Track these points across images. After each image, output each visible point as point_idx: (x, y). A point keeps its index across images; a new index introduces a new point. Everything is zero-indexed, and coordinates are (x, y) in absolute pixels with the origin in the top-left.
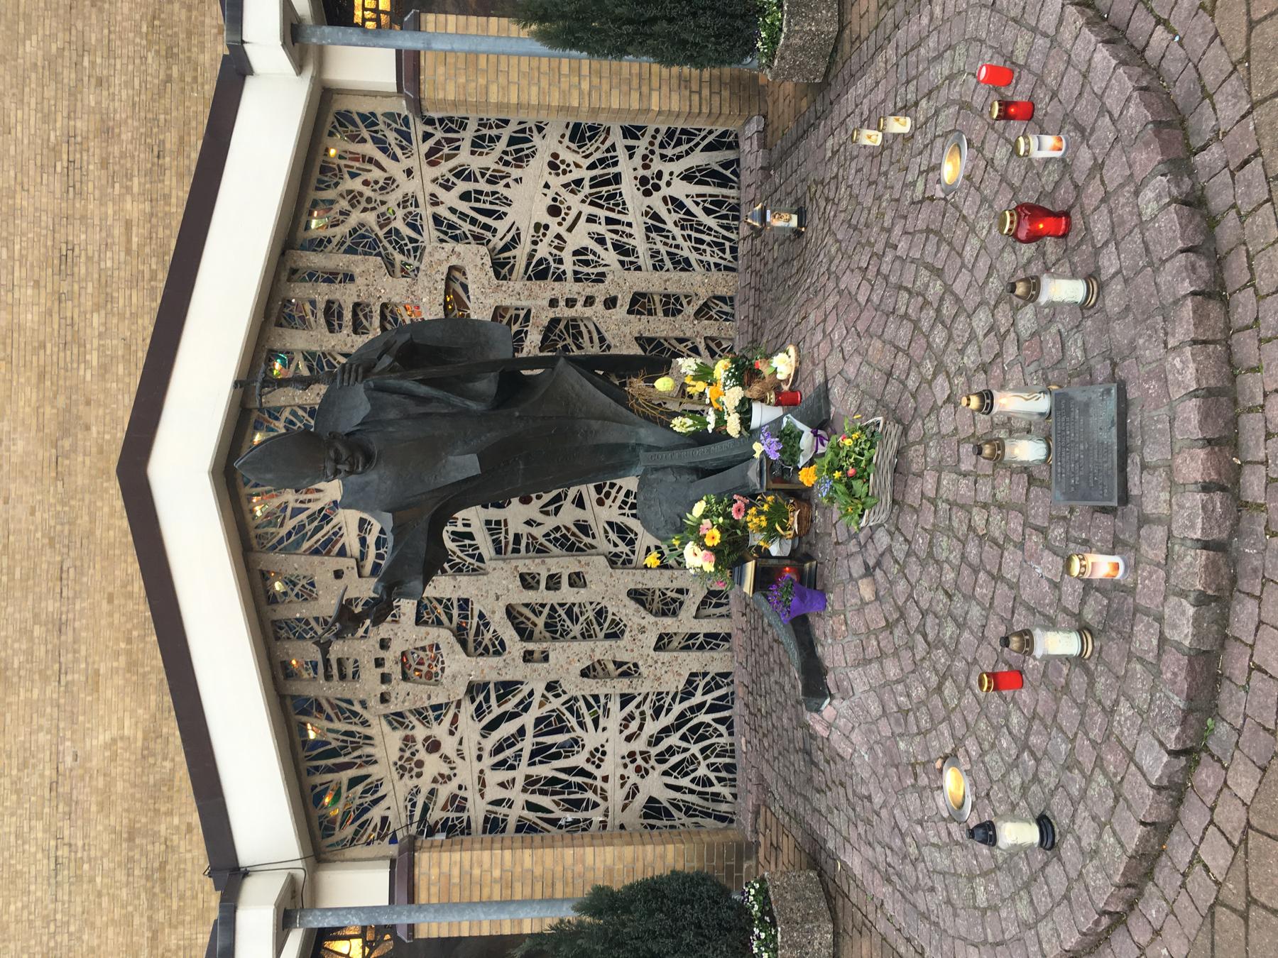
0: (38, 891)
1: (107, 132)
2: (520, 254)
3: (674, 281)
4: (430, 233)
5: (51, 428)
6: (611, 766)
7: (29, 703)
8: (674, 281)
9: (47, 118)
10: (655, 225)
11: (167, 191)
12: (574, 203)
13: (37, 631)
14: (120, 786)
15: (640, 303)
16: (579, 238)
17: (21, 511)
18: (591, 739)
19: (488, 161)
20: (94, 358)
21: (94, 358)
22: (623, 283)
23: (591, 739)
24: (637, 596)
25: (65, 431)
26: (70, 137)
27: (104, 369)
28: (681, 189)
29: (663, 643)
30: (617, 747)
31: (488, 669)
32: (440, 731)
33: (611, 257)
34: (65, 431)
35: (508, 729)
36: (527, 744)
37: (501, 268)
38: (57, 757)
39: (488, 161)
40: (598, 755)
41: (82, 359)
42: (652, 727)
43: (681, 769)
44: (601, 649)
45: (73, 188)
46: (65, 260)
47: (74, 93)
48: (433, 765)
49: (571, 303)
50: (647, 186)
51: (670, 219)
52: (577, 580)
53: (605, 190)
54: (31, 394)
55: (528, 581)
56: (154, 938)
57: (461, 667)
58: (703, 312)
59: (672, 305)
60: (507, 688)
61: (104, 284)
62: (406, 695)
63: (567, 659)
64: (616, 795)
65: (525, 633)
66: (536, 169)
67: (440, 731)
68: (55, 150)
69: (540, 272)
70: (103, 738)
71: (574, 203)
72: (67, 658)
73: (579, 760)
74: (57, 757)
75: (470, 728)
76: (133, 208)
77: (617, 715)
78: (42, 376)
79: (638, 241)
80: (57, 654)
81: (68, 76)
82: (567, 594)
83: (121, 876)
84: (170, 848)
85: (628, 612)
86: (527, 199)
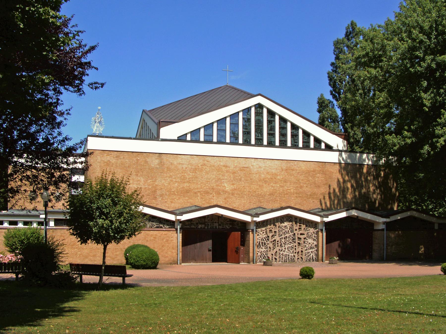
0: (206, 176)
1: (301, 187)
2: (306, 240)
3: (304, 254)
4: (307, 232)
5: (265, 180)
6: (261, 250)
7: (230, 176)
8: (304, 254)
9: (302, 180)
10: (308, 253)
11: (258, 166)
12: (310, 245)
13: (240, 177)
14: (219, 187)
15: (302, 251)
16: (307, 246)
17: (255, 175)
18: (263, 248)
19: (313, 237)
20: (274, 185)
21: (274, 185)
22: (303, 250)
23: (263, 248)
24: (276, 252)
25: (265, 181)
26: (300, 183)
27: (272, 186)
28: (311, 255)
29: (272, 254)
30: (263, 250)
31: (270, 238)
32: (264, 233)
33: (306, 249)
34: (265, 181)
35: (264, 240)
36: (263, 242)
37: (305, 238)
38: (223, 179)
39: (313, 237)
40: (262, 248)
41: (274, 184)
42: (264, 254)
43: (261, 256)
44: (272, 248)
45: (295, 183)
46: (285, 182)
47: (305, 183)
48: (262, 233)
49: (278, 244)
50: (312, 252)
51: (309, 254)
52: (278, 246)
53: (311, 248)
54: (269, 177)
55: (278, 241)
56: (199, 192)
57: (270, 235)
58: (301, 258)
59: (302, 254)
60: (268, 240)
61: (282, 187)
62: (268, 230)
63: (271, 245)
64: (258, 250)
65: (273, 241)
66: (313, 242)
67: (264, 233)
68: (299, 181)
69: (304, 242)
70: (226, 185)
71: (310, 245)
72: (236, 181)
73: (262, 247)
74: (223, 179)
75: (265, 236)
76: (292, 190)
77: (265, 250)
78: (272, 179)
79: (307, 251)
80: (237, 179)
81: (307, 183)
82: (277, 245)
83: (208, 187)
84: (211, 194)
85: (275, 250)
86: (310, 241)
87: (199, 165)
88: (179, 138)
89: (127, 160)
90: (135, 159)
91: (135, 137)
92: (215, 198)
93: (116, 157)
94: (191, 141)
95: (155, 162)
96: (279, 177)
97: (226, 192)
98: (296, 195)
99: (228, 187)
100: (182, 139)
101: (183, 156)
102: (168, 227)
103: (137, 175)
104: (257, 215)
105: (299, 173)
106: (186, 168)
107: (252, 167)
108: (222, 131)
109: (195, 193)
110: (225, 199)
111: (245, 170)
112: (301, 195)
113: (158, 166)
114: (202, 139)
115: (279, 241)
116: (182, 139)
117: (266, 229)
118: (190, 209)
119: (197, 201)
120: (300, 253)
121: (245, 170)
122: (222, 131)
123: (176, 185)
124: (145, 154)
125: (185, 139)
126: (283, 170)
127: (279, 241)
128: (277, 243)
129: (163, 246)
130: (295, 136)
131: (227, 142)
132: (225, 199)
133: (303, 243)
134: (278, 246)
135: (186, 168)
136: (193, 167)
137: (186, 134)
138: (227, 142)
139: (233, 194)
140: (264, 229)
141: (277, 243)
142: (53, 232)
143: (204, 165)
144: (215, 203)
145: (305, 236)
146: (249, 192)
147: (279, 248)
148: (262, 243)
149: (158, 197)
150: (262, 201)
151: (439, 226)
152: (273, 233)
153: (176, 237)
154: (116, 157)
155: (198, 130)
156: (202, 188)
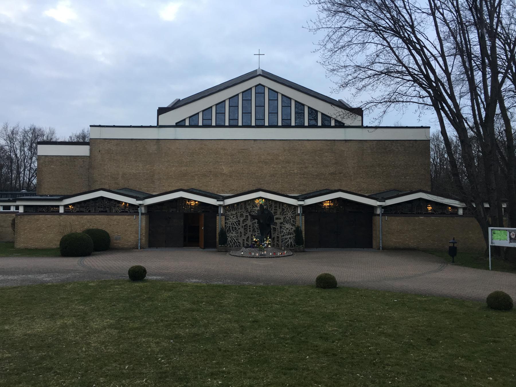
8: (280, 241)
15: (278, 237)
16: (284, 231)
18: (234, 233)
19: (292, 222)
22: (280, 236)
23: (234, 233)
27: (273, 167)
28: (290, 241)
29: (244, 240)
30: (233, 235)
31: (241, 222)
33: (283, 234)
37: (281, 223)
39: (292, 222)
40: (232, 233)
43: (231, 242)
44: (243, 233)
47: (311, 164)
48: (232, 217)
50: (290, 238)
51: (287, 240)
53: (289, 234)
57: (241, 219)
58: (277, 244)
59: (278, 241)
62: (239, 214)
63: (242, 230)
66: (292, 227)
69: (281, 227)
70: (224, 168)
75: (235, 220)
81: (313, 163)
82: (249, 230)
86: (288, 226)
87: (197, 149)
88: (178, 124)
89: (126, 148)
90: (134, 146)
91: (156, 125)
92: (212, 180)
93: (116, 145)
94: (190, 126)
95: (153, 148)
96: (280, 158)
97: (224, 174)
98: (300, 176)
99: (226, 170)
100: (180, 125)
101: (181, 141)
102: (133, 211)
103: (136, 161)
104: (224, 198)
105: (303, 153)
106: (184, 152)
107: (251, 149)
108: (220, 113)
109: (193, 176)
110: (223, 181)
111: (243, 152)
112: (305, 176)
113: (156, 152)
114: (306, 124)
115: (251, 226)
116: (180, 125)
117: (236, 213)
118: (314, 194)
119: (194, 184)
120: (276, 239)
121: (243, 152)
122: (220, 113)
123: (174, 169)
124: (258, 141)
125: (184, 124)
126: (285, 151)
127: (251, 226)
128: (248, 227)
129: (125, 231)
130: (300, 114)
131: (319, 125)
132: (223, 181)
133: (279, 228)
134: (250, 231)
135: (184, 152)
136: (190, 151)
137: (185, 120)
138: (319, 125)
139: (231, 176)
140: (234, 213)
141: (248, 227)
142: (21, 218)
143: (202, 148)
144: (339, 188)
145: (282, 221)
146: (248, 173)
147: (251, 233)
148: (233, 227)
149: (155, 181)
150: (262, 183)
151: (65, 210)
152: (244, 218)
153: (140, 223)
154: (116, 145)
155: (197, 116)
156: (199, 171)
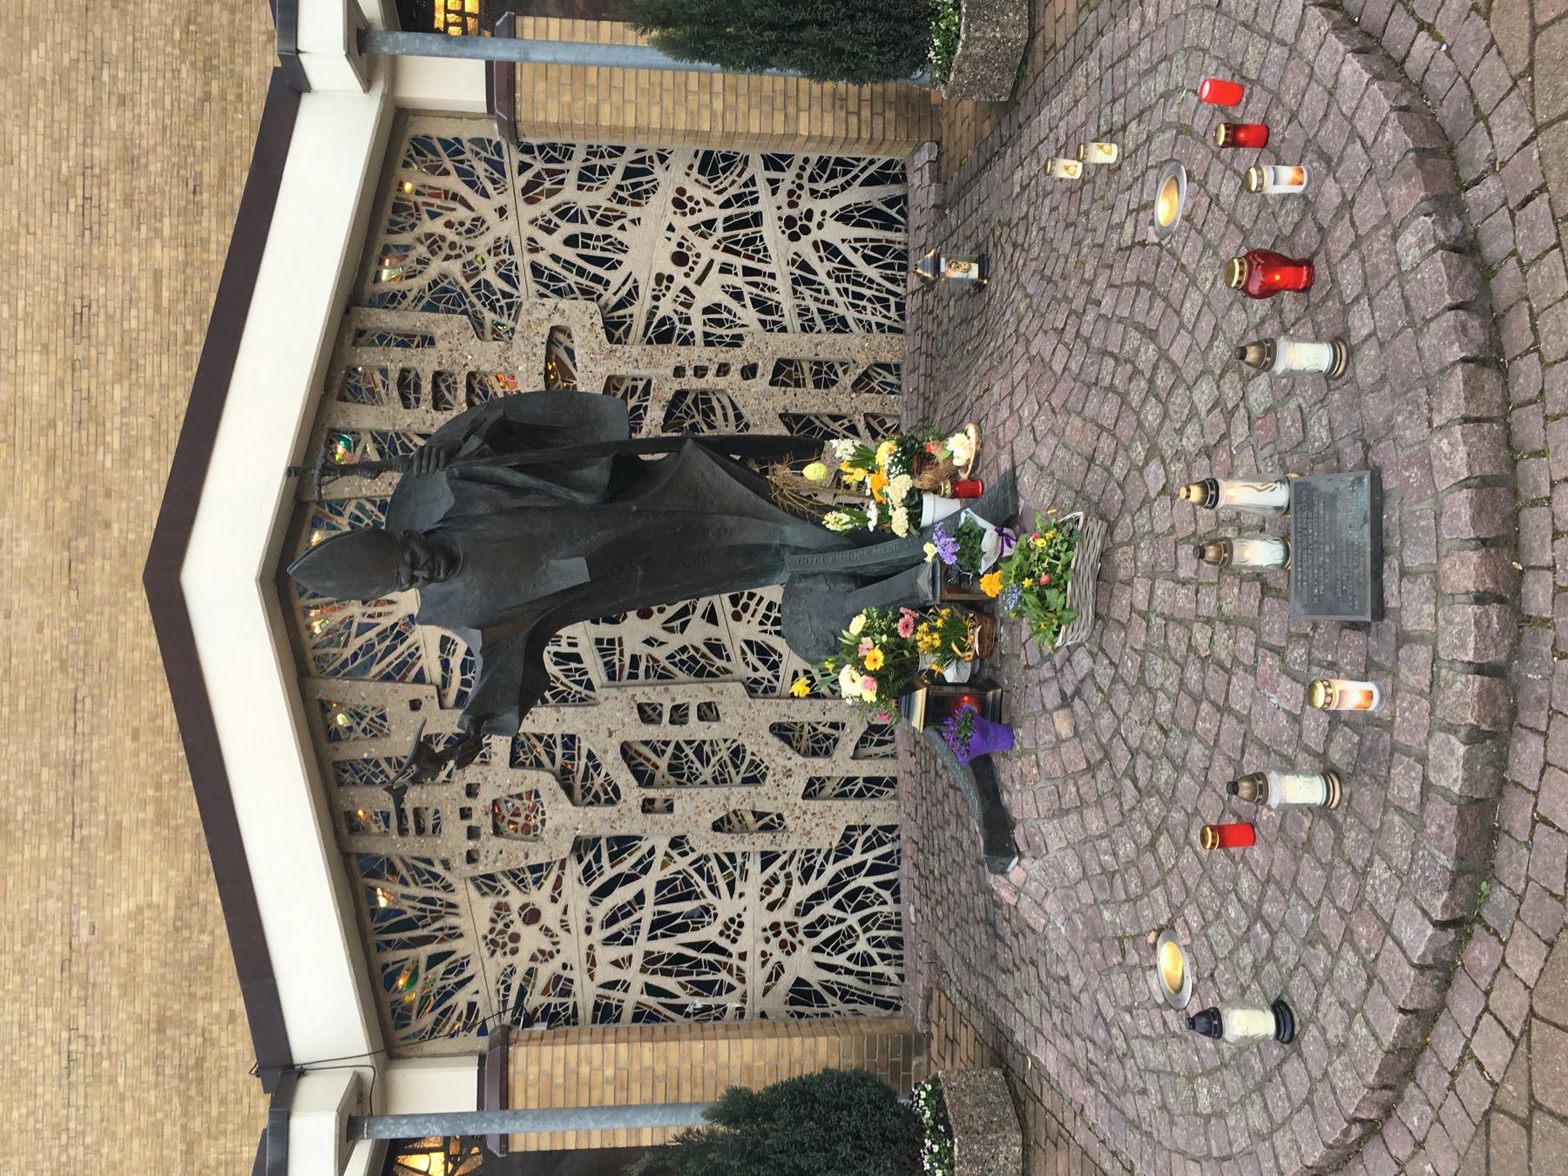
0: (46, 1093)
1: (131, 162)
2: (638, 311)
3: (827, 345)
4: (527, 286)
5: (62, 525)
6: (750, 940)
7: (35, 862)
8: (827, 345)
9: (58, 145)
10: (803, 277)
11: (204, 234)
12: (704, 249)
13: (46, 775)
14: (147, 965)
15: (785, 372)
16: (711, 292)
17: (26, 627)
18: (726, 907)
19: (599, 197)
20: (115, 440)
21: (115, 440)
22: (764, 348)
23: (726, 907)
24: (782, 731)
25: (80, 529)
26: (86, 168)
27: (128, 453)
28: (835, 233)
29: (813, 789)
30: (757, 917)
31: (598, 821)
32: (539, 897)
33: (749, 315)
34: (80, 529)
35: (623, 894)
36: (647, 914)
37: (615, 328)
38: (70, 930)
39: (599, 197)
40: (734, 927)
41: (100, 441)
42: (800, 893)
43: (835, 944)
44: (738, 797)
45: (89, 230)
46: (79, 319)
47: (90, 114)
48: (531, 939)
49: (700, 372)
50: (794, 228)
51: (822, 269)
52: (708, 712)
53: (742, 233)
54: (37, 483)
55: (648, 714)
56: (189, 1152)
57: (565, 819)
58: (862, 383)
59: (824, 375)
60: (622, 845)
61: (128, 349)
62: (498, 854)
63: (695, 809)
64: (756, 976)
65: (644, 778)
66: (658, 207)
67: (539, 897)
68: (68, 184)
69: (663, 334)
70: (126, 905)
71: (704, 249)
72: (82, 808)
73: (710, 933)
74: (70, 930)
75: (576, 894)
76: (163, 256)
77: (757, 878)
78: (51, 462)
79: (783, 296)
80: (70, 802)
81: (84, 93)
82: (695, 729)
83: (148, 1075)
84: (208, 1041)
85: (771, 751)
86: (647, 245)
